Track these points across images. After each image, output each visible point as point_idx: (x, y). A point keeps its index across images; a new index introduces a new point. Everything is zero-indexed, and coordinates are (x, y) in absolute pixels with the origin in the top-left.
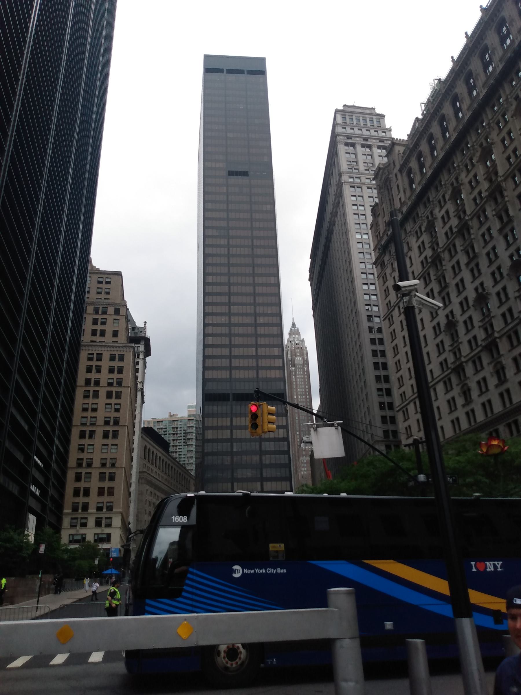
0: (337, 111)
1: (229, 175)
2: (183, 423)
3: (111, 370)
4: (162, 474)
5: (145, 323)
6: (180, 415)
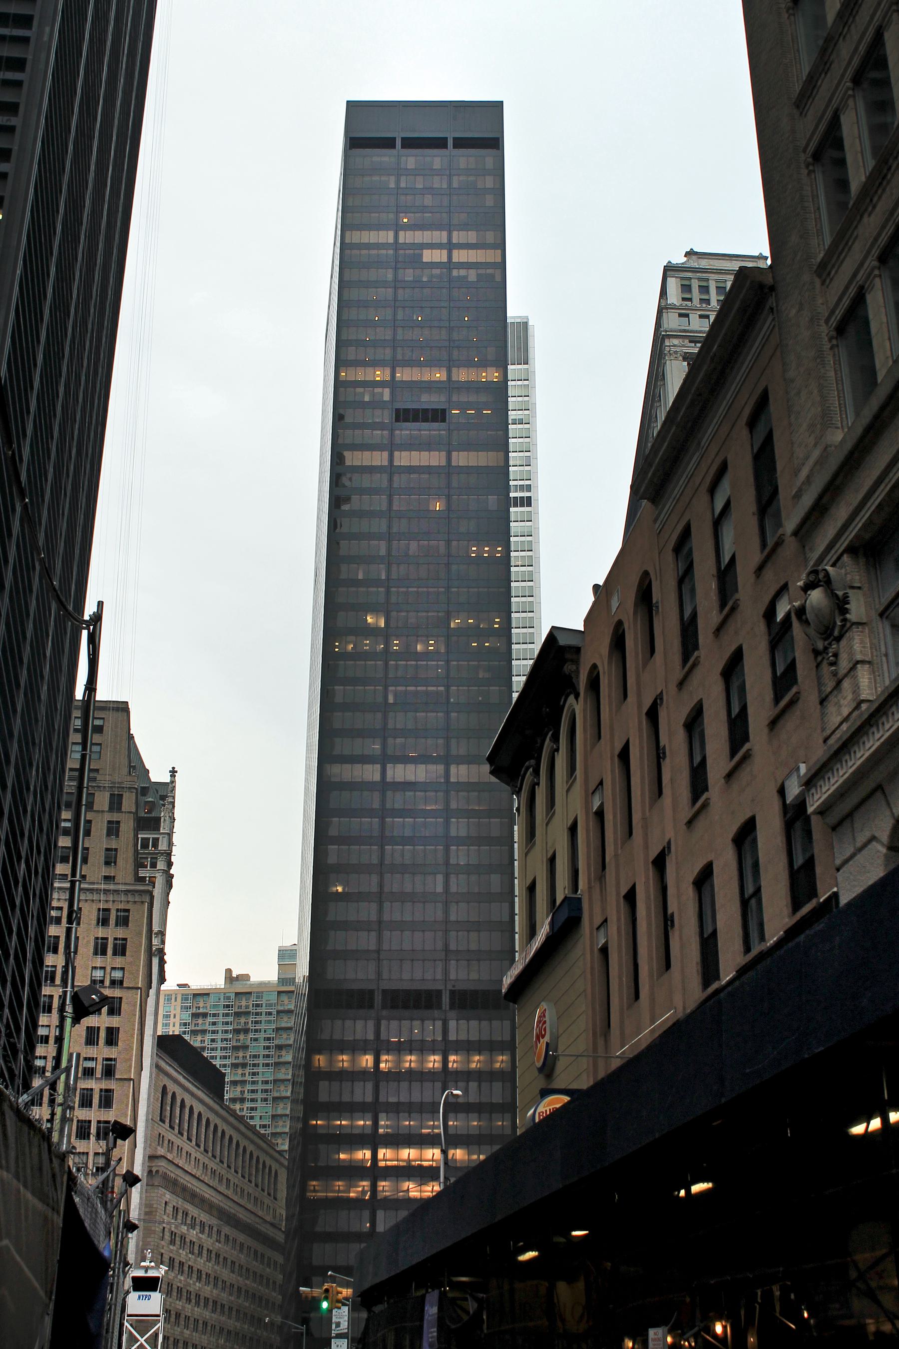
0: (669, 270)
1: (397, 420)
2: (264, 1002)
3: (100, 948)
4: (203, 1159)
5: (173, 772)
6: (256, 977)
